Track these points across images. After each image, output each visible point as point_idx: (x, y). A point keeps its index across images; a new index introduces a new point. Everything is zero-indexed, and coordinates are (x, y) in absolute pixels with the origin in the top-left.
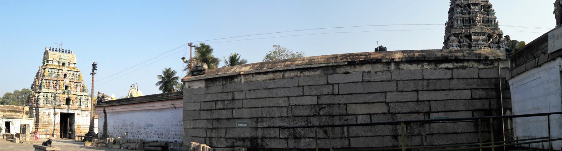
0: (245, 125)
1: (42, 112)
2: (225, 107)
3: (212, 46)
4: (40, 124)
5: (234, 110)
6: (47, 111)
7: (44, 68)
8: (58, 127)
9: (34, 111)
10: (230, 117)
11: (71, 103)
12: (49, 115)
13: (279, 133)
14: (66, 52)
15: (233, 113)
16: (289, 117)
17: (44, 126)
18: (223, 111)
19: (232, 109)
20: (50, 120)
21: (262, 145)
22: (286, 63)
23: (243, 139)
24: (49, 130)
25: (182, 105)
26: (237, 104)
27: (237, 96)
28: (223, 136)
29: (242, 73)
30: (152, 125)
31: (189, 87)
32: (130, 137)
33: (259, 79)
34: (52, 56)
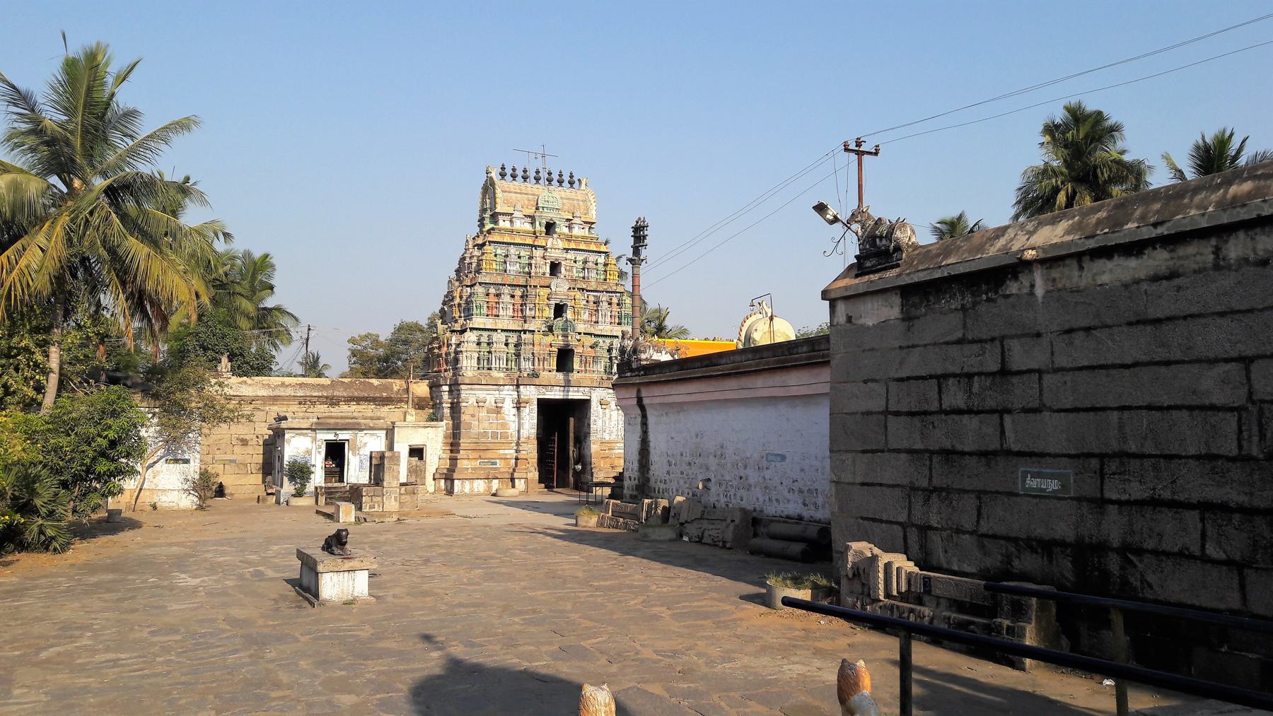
0: (1052, 485)
1: (472, 400)
2: (976, 403)
3: (1113, 116)
4: (464, 442)
5: (1007, 419)
6: (490, 396)
7: (480, 241)
8: (531, 451)
9: (446, 396)
10: (995, 445)
11: (576, 366)
12: (498, 410)
13: (1203, 535)
14: (560, 182)
15: (1003, 432)
16: (1249, 459)
17: (480, 449)
18: (966, 418)
19: (1002, 412)
20: (504, 425)
21: (1125, 582)
22: (1234, 189)
23: (1047, 547)
24: (499, 464)
25: (826, 389)
26: (1022, 392)
27: (1020, 357)
28: (968, 522)
29: (1030, 254)
30: (783, 458)
31: (849, 319)
32: (716, 496)
33: (1105, 278)
34: (510, 196)
